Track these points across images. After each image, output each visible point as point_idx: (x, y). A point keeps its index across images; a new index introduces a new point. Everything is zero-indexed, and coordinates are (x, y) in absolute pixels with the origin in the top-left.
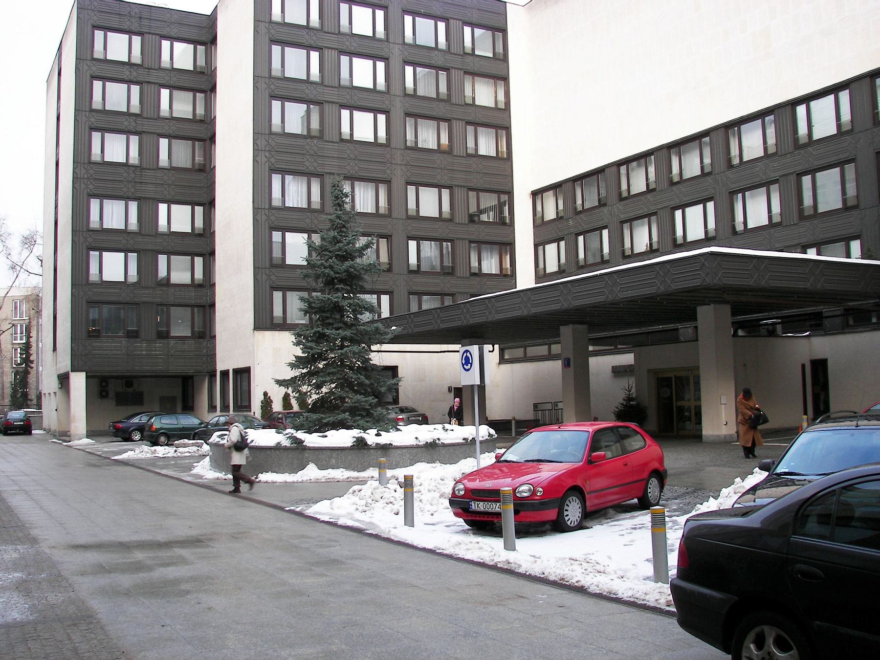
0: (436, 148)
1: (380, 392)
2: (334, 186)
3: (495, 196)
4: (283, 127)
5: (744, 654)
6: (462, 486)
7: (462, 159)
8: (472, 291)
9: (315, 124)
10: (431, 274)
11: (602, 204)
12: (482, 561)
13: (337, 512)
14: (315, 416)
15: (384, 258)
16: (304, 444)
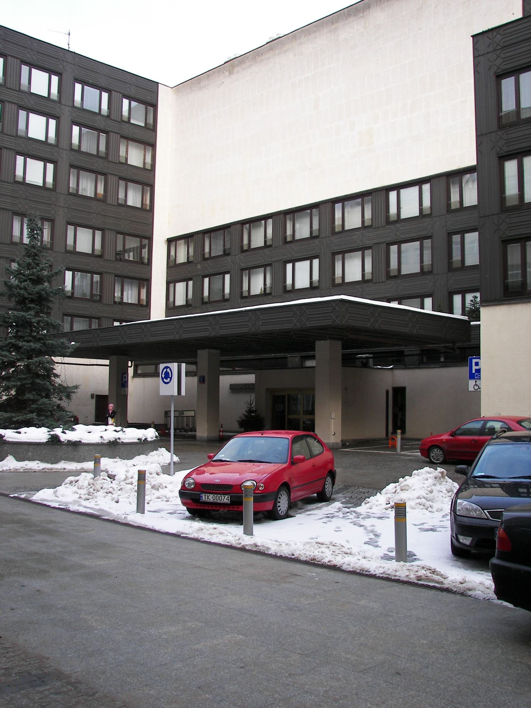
0: (93, 196)
3: (138, 240)
7: (113, 207)
8: (129, 317)
10: (82, 299)
11: (226, 253)
12: (229, 544)
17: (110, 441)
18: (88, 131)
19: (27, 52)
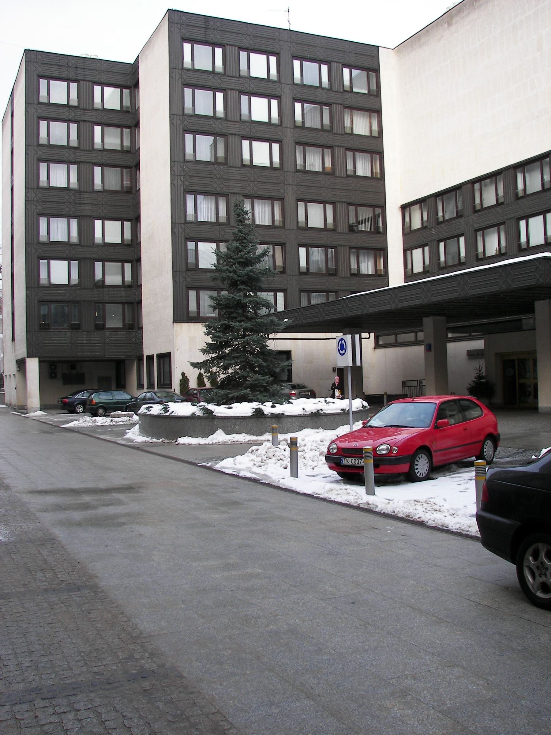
1: (275, 372)
2: (236, 206)
4: (195, 156)
5: (525, 564)
6: (335, 446)
8: (354, 288)
9: (221, 153)
10: (319, 274)
11: (459, 215)
12: (348, 503)
13: (239, 466)
14: (222, 392)
15: (279, 262)
16: (214, 414)
17: (312, 413)
18: (314, 107)
19: (243, 38)
